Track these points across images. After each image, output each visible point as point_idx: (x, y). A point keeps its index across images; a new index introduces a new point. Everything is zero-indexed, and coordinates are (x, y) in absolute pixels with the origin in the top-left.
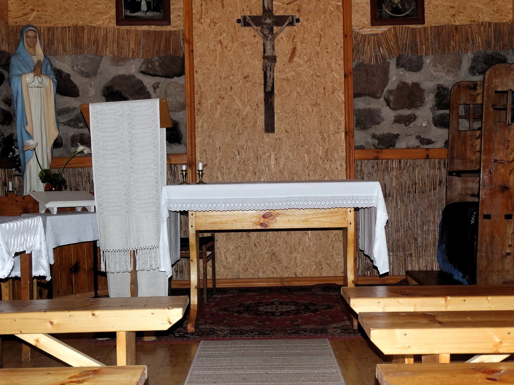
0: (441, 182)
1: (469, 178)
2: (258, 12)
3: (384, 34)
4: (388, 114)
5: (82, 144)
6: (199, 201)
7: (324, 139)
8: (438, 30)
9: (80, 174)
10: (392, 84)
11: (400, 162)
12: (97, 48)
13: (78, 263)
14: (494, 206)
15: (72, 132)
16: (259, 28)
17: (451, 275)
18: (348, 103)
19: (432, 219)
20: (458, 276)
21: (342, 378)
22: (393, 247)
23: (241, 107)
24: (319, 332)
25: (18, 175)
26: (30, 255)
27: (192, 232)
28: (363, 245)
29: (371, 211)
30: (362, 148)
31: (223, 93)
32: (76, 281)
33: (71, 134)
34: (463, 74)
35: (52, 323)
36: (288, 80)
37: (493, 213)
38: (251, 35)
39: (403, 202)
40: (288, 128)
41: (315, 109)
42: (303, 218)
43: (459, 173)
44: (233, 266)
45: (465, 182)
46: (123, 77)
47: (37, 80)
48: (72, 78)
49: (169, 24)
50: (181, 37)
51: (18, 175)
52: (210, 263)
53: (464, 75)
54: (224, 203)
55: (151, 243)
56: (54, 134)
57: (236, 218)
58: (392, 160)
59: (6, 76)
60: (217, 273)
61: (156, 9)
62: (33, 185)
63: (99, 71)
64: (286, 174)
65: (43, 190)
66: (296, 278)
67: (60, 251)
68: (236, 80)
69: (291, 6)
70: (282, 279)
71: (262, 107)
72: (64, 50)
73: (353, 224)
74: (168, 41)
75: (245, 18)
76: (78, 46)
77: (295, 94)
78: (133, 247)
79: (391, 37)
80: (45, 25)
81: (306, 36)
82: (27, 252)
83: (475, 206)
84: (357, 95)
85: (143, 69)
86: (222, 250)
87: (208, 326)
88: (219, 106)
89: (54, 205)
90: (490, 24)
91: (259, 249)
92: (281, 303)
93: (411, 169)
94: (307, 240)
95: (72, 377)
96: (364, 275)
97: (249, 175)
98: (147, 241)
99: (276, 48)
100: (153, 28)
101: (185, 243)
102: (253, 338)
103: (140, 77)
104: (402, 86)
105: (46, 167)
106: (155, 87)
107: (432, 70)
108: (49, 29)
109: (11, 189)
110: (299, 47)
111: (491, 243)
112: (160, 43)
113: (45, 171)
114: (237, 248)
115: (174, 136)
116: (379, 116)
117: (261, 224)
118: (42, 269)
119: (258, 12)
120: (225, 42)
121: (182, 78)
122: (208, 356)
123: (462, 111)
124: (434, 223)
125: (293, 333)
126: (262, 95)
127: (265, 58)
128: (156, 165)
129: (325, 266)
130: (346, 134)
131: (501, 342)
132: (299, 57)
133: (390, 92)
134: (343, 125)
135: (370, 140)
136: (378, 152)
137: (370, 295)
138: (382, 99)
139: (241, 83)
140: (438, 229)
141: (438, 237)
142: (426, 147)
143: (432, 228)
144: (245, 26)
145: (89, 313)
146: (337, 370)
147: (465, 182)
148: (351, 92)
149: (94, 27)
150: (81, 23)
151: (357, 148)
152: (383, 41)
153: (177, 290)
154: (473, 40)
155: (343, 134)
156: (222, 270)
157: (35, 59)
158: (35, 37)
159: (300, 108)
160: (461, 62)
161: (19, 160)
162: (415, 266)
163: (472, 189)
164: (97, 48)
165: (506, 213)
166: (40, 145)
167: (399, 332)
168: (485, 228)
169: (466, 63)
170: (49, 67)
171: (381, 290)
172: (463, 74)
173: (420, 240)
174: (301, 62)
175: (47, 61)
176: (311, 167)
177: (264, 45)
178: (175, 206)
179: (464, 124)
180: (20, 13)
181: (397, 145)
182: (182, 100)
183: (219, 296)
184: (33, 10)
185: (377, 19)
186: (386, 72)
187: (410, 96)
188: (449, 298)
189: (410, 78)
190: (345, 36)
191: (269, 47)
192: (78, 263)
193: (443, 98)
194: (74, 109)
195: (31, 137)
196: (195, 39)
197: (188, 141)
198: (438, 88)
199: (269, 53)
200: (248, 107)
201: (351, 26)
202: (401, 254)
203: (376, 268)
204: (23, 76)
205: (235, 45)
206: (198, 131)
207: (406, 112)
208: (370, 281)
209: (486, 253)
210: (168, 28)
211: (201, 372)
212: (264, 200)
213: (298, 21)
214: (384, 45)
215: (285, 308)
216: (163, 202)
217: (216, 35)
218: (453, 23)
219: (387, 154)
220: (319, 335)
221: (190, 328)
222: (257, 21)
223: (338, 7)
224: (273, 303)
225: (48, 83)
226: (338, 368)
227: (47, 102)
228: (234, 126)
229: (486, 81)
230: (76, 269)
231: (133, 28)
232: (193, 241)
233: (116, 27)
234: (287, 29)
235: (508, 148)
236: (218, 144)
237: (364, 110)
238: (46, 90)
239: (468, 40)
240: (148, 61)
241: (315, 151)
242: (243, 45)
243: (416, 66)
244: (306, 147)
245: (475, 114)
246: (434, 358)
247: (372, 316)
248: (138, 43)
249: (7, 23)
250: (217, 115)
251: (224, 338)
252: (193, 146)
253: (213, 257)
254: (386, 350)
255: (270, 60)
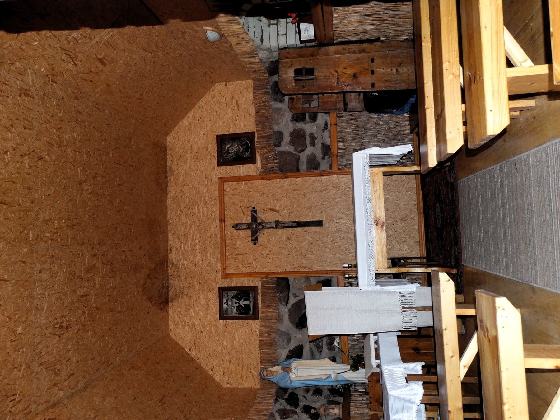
0: (351, 115)
1: (348, 99)
2: (249, 232)
3: (261, 155)
4: (309, 150)
5: (333, 344)
6: (369, 266)
7: (326, 190)
8: (259, 123)
9: (352, 346)
10: (291, 149)
11: (339, 141)
12: (273, 332)
13: (413, 349)
14: (366, 82)
15: (325, 350)
16: (259, 231)
17: (412, 104)
18: (303, 176)
19: (375, 119)
20: (412, 100)
21: (484, 171)
22: (395, 143)
23: (306, 242)
24: (453, 187)
25: (355, 386)
26: (408, 374)
27: (388, 271)
28: (394, 161)
29: (372, 157)
30: (331, 166)
31: (298, 253)
32: (425, 350)
33: (327, 350)
34: (284, 107)
35: (452, 357)
36: (289, 213)
37: (371, 82)
38: (263, 236)
39: (364, 138)
40: (319, 212)
41: (307, 196)
42: (378, 200)
43: (345, 105)
44: (413, 246)
45: (351, 100)
46: (290, 316)
47: (293, 370)
48: (291, 349)
49: (257, 287)
50: (265, 279)
51: (355, 386)
52: (409, 261)
53: (284, 106)
54: (371, 250)
55: (397, 296)
56: (327, 361)
57: (379, 243)
58: (338, 146)
59: (292, 391)
60: (416, 256)
61: (248, 295)
62: (360, 376)
63: (286, 331)
64: (349, 213)
65: (364, 370)
66: (418, 204)
67: (405, 359)
68: (290, 245)
69: (245, 212)
70: (419, 214)
71: (307, 228)
72: (274, 353)
73: (380, 168)
74: (268, 288)
75: (252, 240)
76: (270, 345)
77: (299, 208)
78: (400, 309)
79: (262, 151)
80: (259, 365)
81: (262, 203)
82: (406, 376)
83: (365, 93)
84: (298, 170)
85: (285, 304)
86: (400, 253)
87: (452, 260)
88: (307, 256)
89: (374, 362)
90: (254, 93)
91: (398, 229)
92: (435, 213)
93: (343, 134)
94: (392, 198)
95: (485, 336)
96: (414, 160)
97: (350, 236)
98: (397, 300)
99: (270, 221)
100: (260, 297)
101: (396, 276)
102: (459, 230)
103: (289, 305)
104: (292, 142)
105: (349, 367)
106: (295, 296)
107: (281, 125)
108: (262, 362)
109: (364, 390)
110: (269, 207)
111: (389, 81)
112: (268, 293)
113: (351, 367)
114: (398, 243)
115: (327, 283)
116: (311, 156)
117: (382, 226)
118: (417, 368)
119: (249, 232)
120: (267, 252)
121: (289, 279)
122: (472, 259)
123: (307, 106)
124: (378, 118)
125: (455, 204)
126: (299, 229)
127: (276, 228)
128: (346, 293)
129: (409, 186)
130: (322, 176)
131: (453, 74)
132: (275, 206)
133: (296, 150)
134: (317, 177)
135: (325, 161)
136: (333, 155)
137: (426, 155)
138: (300, 154)
139: (292, 242)
140: (382, 115)
141: (387, 115)
142: (329, 126)
143: (381, 119)
144: (257, 240)
145: (445, 333)
146: (478, 174)
147: (351, 100)
148: (296, 173)
149: (260, 334)
150: (258, 342)
151: (331, 168)
152: (265, 156)
153: (429, 280)
154: (264, 102)
155: (322, 177)
156: (414, 252)
157: (281, 371)
158: (267, 371)
159: (307, 205)
160: (277, 109)
161: (345, 385)
162: (407, 128)
163: (355, 96)
164: (273, 332)
165: (370, 74)
166: (335, 371)
167: (449, 136)
168: (381, 86)
169: (278, 105)
170: (285, 363)
171: (422, 149)
172: (284, 107)
173: (389, 126)
174: (278, 205)
175: (281, 364)
176: (344, 197)
177: (269, 228)
178: (372, 281)
179: (315, 104)
180: (253, 380)
181: (329, 143)
182: (303, 279)
183: (432, 254)
184: (251, 372)
185: (252, 160)
186: (283, 153)
187: (298, 138)
188: (426, 107)
189: (287, 138)
190: (263, 179)
191: (270, 225)
192: (413, 349)
193: (299, 117)
194: (310, 348)
195: (330, 376)
196: (266, 270)
197: (329, 275)
198: (293, 121)
199: (274, 225)
200: (307, 237)
201: (256, 176)
202: (399, 137)
203: (409, 152)
204: (291, 379)
205: (269, 246)
206: (323, 269)
207: (308, 140)
208: (416, 156)
209: (397, 84)
210: (260, 287)
211: (484, 263)
212: (367, 224)
213: (254, 208)
214: (268, 155)
215: (438, 210)
216: (370, 289)
217: (263, 258)
218: (254, 115)
219: (334, 150)
220: (455, 187)
221: (454, 271)
222: (254, 233)
223: (245, 184)
224: (435, 219)
225: (295, 363)
226: (477, 173)
227: (307, 365)
228: (319, 246)
229: (289, 93)
230: (416, 350)
231: (260, 310)
232: (394, 271)
233: (259, 320)
234: (259, 214)
235: (330, 76)
236: (331, 256)
237: (307, 165)
238: (300, 365)
239: (264, 105)
240: (280, 299)
241: (334, 195)
242: (269, 241)
243: (280, 135)
244: (331, 200)
245: (308, 96)
246: (465, 114)
247: (439, 153)
248: (269, 306)
249: (259, 389)
250: (312, 257)
251: (460, 249)
252: (332, 272)
253: (405, 259)
254: (461, 143)
255: (278, 225)
